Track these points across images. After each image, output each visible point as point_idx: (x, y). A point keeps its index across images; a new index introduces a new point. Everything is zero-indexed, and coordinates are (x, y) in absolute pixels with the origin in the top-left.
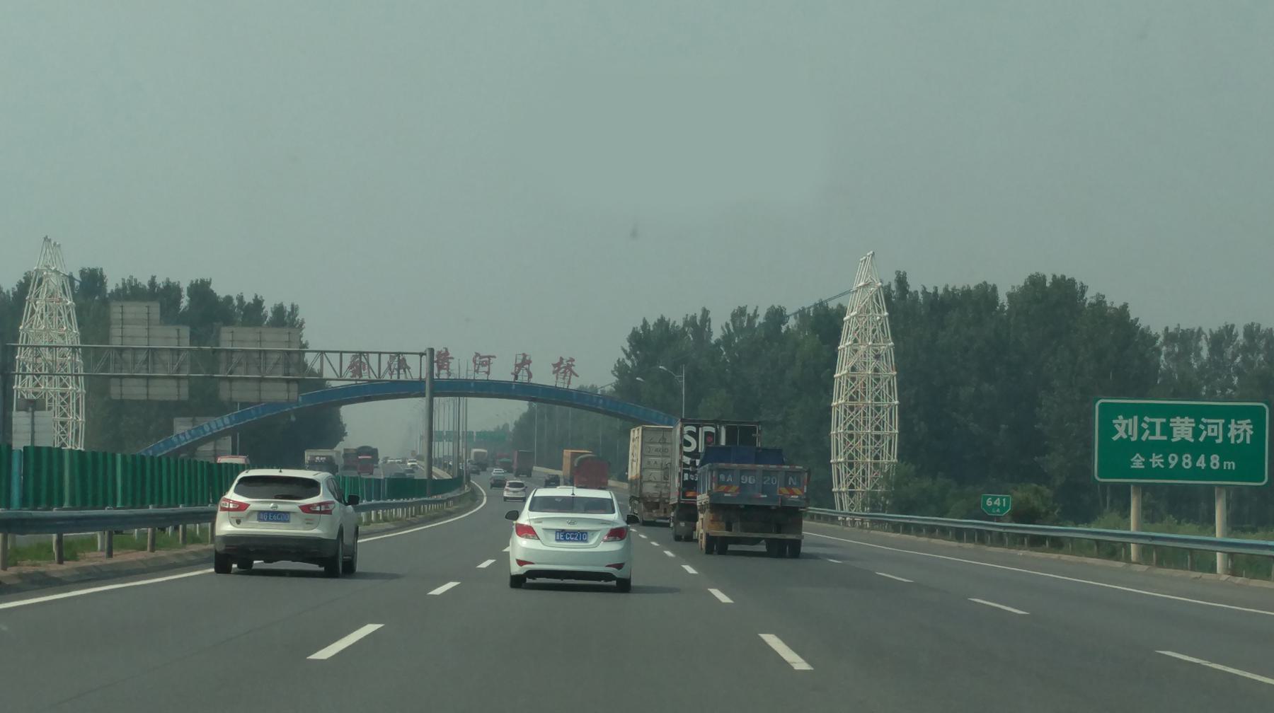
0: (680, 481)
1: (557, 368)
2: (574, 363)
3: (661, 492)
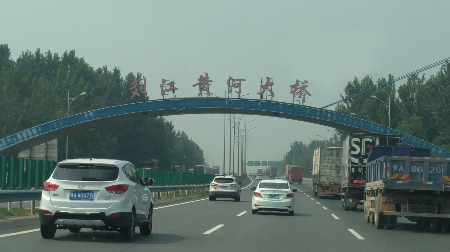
0: (349, 173)
1: (293, 89)
2: (307, 84)
3: (330, 182)
